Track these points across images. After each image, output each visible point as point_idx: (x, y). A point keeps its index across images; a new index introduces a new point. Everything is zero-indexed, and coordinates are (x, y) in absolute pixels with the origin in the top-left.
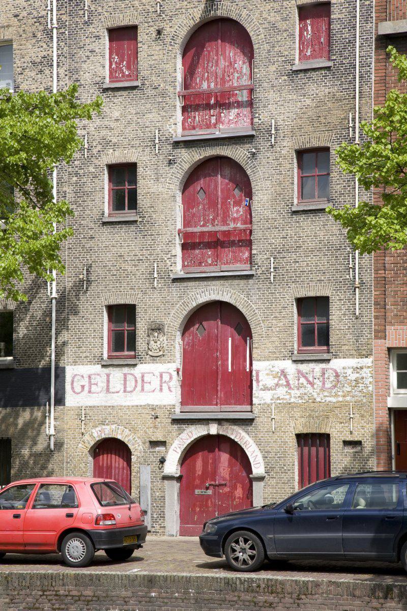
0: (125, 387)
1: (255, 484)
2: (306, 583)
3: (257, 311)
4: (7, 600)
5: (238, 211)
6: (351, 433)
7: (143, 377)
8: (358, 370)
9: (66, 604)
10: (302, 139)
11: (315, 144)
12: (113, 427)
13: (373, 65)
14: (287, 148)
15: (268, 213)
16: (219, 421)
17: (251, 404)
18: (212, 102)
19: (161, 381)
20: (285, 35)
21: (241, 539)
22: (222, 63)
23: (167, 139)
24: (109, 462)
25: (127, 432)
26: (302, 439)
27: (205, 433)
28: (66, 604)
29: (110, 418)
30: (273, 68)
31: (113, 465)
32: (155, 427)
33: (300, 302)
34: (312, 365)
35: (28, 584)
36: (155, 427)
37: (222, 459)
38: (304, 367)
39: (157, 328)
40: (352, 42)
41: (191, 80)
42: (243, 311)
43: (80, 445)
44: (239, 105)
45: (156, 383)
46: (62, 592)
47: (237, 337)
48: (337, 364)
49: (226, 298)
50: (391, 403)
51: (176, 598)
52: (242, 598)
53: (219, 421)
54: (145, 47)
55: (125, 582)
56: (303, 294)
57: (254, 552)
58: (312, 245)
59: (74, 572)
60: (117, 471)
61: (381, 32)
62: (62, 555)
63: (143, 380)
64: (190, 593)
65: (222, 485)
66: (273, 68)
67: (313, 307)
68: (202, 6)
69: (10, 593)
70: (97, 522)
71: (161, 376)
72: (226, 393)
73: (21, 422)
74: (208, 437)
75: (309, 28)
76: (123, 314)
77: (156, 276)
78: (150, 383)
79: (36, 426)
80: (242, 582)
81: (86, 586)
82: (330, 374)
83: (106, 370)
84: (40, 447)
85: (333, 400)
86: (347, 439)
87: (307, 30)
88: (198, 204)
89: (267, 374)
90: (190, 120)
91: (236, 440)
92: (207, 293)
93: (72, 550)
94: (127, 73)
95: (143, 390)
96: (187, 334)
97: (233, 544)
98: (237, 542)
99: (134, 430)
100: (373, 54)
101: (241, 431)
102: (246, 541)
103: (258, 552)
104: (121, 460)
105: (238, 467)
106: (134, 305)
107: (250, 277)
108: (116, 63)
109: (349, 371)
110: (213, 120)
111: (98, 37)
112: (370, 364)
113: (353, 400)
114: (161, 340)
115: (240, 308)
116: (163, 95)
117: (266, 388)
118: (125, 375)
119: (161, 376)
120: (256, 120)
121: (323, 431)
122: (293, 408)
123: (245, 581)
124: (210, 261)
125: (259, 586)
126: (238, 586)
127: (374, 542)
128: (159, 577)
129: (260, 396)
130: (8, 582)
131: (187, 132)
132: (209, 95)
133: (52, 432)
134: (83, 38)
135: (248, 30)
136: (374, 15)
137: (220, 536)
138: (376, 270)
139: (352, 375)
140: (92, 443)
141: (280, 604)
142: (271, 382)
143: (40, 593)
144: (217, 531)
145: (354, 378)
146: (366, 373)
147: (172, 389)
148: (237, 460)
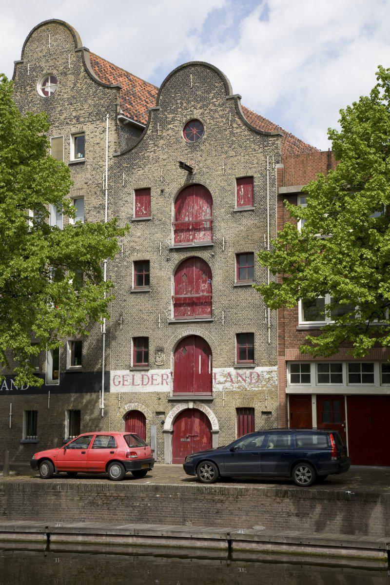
4: (78, 498)
7: (152, 376)
8: (270, 373)
10: (239, 247)
11: (246, 250)
12: (136, 404)
14: (231, 252)
15: (221, 287)
16: (194, 401)
17: (211, 391)
18: (191, 228)
22: (196, 207)
25: (143, 407)
27: (186, 407)
30: (223, 210)
32: (159, 404)
33: (238, 336)
34: (245, 370)
36: (159, 404)
38: (241, 371)
39: (160, 350)
40: (265, 197)
44: (205, 229)
45: (159, 380)
46: (108, 494)
48: (258, 369)
49: (198, 334)
51: (170, 498)
52: (206, 498)
56: (240, 331)
63: (152, 379)
66: (223, 210)
67: (246, 338)
70: (127, 456)
73: (85, 401)
74: (188, 410)
75: (242, 189)
76: (141, 342)
82: (255, 376)
83: (132, 373)
87: (241, 191)
89: (220, 375)
95: (152, 384)
97: (202, 468)
99: (147, 406)
102: (208, 467)
103: (215, 473)
104: (140, 422)
105: (204, 426)
106: (148, 337)
109: (265, 374)
110: (191, 237)
111: (129, 194)
112: (276, 370)
117: (220, 383)
118: (143, 375)
121: (251, 406)
124: (189, 313)
125: (215, 491)
127: (277, 466)
131: (177, 244)
136: (276, 183)
138: (280, 319)
140: (125, 413)
142: (222, 379)
146: (274, 374)
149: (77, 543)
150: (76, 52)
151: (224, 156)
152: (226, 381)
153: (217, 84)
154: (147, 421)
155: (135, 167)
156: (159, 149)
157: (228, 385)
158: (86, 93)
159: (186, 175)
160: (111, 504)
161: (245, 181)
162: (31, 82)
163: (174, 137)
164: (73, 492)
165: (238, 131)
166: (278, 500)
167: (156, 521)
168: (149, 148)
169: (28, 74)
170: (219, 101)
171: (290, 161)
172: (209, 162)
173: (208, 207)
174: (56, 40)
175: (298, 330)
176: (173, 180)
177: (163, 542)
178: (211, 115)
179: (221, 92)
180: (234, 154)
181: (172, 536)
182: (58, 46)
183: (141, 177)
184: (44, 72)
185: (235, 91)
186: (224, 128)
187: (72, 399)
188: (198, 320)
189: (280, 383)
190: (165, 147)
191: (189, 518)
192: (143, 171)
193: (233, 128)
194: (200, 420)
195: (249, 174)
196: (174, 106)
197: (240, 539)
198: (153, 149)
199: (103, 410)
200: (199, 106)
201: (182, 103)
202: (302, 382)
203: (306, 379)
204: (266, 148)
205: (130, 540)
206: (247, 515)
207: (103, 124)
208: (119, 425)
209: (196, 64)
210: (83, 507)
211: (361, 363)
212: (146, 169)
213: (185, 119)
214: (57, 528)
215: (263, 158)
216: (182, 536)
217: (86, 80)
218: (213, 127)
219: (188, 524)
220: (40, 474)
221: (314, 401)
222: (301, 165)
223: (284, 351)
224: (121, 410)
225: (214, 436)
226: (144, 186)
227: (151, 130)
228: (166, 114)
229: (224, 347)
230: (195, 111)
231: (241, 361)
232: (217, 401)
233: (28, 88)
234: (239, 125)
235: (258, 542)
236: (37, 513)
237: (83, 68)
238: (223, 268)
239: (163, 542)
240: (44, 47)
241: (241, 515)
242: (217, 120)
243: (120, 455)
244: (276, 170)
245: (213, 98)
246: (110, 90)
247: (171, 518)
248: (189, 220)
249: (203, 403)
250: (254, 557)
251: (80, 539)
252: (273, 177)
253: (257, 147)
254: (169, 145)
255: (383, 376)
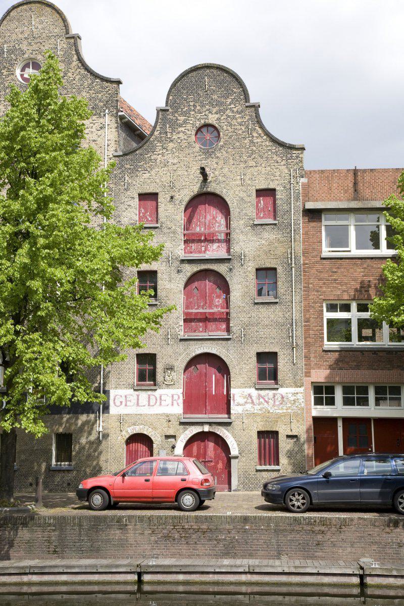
0: (149, 403)
1: (232, 460)
2: (345, 519)
3: (233, 359)
4: (150, 532)
5: (218, 301)
6: (291, 430)
7: (161, 397)
8: (295, 395)
9: (189, 534)
10: (260, 262)
11: (268, 265)
12: (142, 426)
13: (301, 225)
14: (251, 267)
15: (240, 303)
16: (210, 424)
17: (228, 412)
18: (203, 238)
19: (173, 399)
20: (249, 204)
21: (296, 493)
22: (208, 217)
23: (176, 258)
24: (136, 448)
25: (150, 430)
26: (261, 434)
27: (201, 430)
28: (189, 534)
29: (140, 422)
30: (242, 222)
31: (139, 449)
32: (169, 427)
33: (259, 355)
34: (267, 391)
35: (164, 522)
36: (169, 427)
37: (210, 446)
38: (263, 393)
39: (171, 368)
40: (289, 211)
41: (189, 226)
42: (225, 359)
43: (119, 438)
44: (219, 241)
45: (169, 401)
46: (186, 527)
47: (218, 374)
48: (282, 391)
49: (214, 351)
50: (315, 413)
51: (262, 529)
52: (304, 529)
53: (210, 424)
54: (163, 205)
55: (228, 520)
56: (261, 350)
57: (305, 501)
58: (267, 323)
59: (194, 514)
60: (141, 454)
61: (307, 207)
62: (179, 504)
63: (161, 399)
64: (271, 526)
65: (209, 461)
66: (242, 222)
67: (267, 359)
68: (199, 185)
69: (152, 527)
70: (202, 484)
71: (173, 396)
72: (211, 407)
73: (80, 422)
74: (203, 433)
75: (262, 202)
76: (147, 360)
77: (169, 337)
78: (165, 400)
79: (91, 425)
80: (304, 519)
81: (202, 522)
82: (279, 397)
83: (137, 393)
84: (93, 438)
85: (281, 411)
86: (289, 434)
87: (260, 203)
88: (194, 296)
89: (240, 396)
90: (188, 248)
91: (220, 435)
92: (202, 348)
93: (95, 502)
94: (150, 219)
95: (161, 404)
96: (186, 372)
97: (291, 497)
98: (294, 495)
99: (155, 429)
100: (301, 219)
101: (223, 429)
102: (299, 494)
103: (307, 501)
104: (144, 447)
105: (219, 450)
106: (155, 355)
107: (229, 339)
108: (143, 213)
109: (290, 395)
110: (203, 249)
111: (133, 198)
112: (302, 391)
113: (292, 411)
114: (173, 375)
115: (223, 357)
116: (174, 233)
117: (239, 405)
118: (149, 396)
119: (173, 396)
120: (232, 250)
121: (274, 430)
122: (255, 416)
123: (306, 518)
124: (201, 329)
125: (315, 521)
126: (302, 521)
127: (381, 494)
128: (251, 517)
129: (234, 409)
130: (150, 520)
131: (187, 255)
132: (200, 235)
133: (101, 429)
134: (123, 198)
135: (227, 200)
136: (301, 198)
137: (283, 492)
138: (305, 338)
139: (291, 397)
140: (127, 436)
141: (329, 532)
142: (242, 401)
143: (173, 527)
144: (281, 489)
145: (292, 399)
146: (300, 396)
147: (179, 404)
148: (219, 446)
149: (178, 583)
150: (67, 38)
151: (242, 165)
152: (246, 402)
153: (235, 90)
154: (155, 446)
155: (140, 169)
156: (168, 152)
157: (249, 406)
158: (79, 85)
159: (200, 181)
160: (190, 537)
161: (267, 193)
162: (8, 65)
163: (185, 141)
164: (143, 525)
165: (259, 141)
166: (387, 530)
167: (245, 556)
168: (157, 150)
169: (5, 56)
170: (238, 107)
171: (315, 176)
172: (226, 170)
173: (222, 218)
174: (41, 22)
175: (324, 351)
176: (183, 188)
177: (284, 579)
178: (229, 120)
179: (240, 98)
180: (255, 165)
181: (295, 572)
182: (43, 29)
183: (146, 181)
184: (26, 56)
185: (253, 100)
186: (243, 136)
187: (65, 419)
188: (212, 337)
189: (306, 404)
190: (175, 151)
191: (285, 551)
192: (150, 174)
193: (253, 137)
194: (215, 444)
195: (271, 186)
196: (186, 108)
197: (375, 573)
198: (161, 151)
199: (101, 433)
200: (214, 110)
201: (195, 106)
202: (357, 405)
203: (331, 402)
204: (290, 161)
205: (244, 578)
206: (352, 546)
207: (101, 120)
208: (121, 450)
209: (212, 67)
210: (156, 542)
211: (388, 385)
212: (153, 172)
213: (199, 123)
214: (153, 566)
215: (286, 171)
216: (307, 572)
217: (79, 70)
218: (231, 134)
219: (284, 558)
220: (90, 503)
221: (340, 424)
222: (326, 182)
223: (310, 372)
224: (124, 433)
225: (233, 461)
226: (151, 191)
227: (159, 132)
228: (176, 115)
229: (243, 367)
230: (210, 116)
231: (261, 382)
232: (237, 424)
233: (5, 72)
234: (260, 135)
235: (395, 577)
236: (98, 550)
237: (75, 57)
238: (242, 284)
239: (284, 579)
240: (26, 28)
241: (345, 547)
242: (235, 127)
243: (193, 483)
244: (300, 184)
245: (230, 104)
246: (109, 84)
247: (263, 552)
248: (200, 230)
249: (220, 426)
250: (392, 593)
251: (181, 577)
252: (297, 191)
253: (279, 159)
254: (180, 149)
255: (344, 398)
